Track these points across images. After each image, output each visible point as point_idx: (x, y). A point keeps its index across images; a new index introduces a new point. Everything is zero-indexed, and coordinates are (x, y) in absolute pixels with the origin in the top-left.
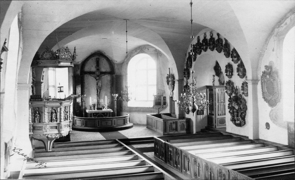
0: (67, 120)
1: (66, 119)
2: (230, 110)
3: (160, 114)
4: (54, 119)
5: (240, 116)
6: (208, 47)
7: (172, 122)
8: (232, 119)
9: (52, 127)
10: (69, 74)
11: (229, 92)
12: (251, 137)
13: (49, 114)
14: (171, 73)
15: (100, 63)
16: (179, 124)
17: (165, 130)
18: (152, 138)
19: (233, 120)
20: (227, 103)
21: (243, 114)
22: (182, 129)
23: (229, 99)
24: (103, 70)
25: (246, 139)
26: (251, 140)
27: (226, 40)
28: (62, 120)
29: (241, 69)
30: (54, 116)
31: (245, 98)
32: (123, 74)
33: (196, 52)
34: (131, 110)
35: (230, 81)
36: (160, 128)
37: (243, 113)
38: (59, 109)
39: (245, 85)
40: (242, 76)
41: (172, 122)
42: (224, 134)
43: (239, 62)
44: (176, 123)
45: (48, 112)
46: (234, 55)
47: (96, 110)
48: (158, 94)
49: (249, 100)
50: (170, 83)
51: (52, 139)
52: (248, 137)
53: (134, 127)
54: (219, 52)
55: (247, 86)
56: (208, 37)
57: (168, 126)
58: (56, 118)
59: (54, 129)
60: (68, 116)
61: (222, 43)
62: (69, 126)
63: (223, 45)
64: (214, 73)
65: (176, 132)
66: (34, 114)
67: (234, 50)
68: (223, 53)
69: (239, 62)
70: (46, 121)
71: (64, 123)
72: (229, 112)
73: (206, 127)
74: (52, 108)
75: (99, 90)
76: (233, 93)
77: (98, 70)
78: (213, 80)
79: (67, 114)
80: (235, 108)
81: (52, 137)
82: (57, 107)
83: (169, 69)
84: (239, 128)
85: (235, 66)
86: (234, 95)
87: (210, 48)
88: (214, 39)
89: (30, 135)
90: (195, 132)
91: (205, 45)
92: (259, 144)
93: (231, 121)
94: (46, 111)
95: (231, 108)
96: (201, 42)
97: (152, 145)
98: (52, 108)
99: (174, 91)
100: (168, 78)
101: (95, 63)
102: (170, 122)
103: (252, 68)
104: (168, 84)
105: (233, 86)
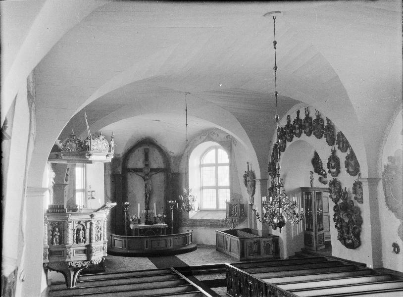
0: (100, 240)
3: (235, 230)
4: (82, 238)
6: (303, 131)
8: (339, 237)
9: (78, 252)
11: (334, 197)
12: (370, 266)
13: (74, 231)
14: (250, 170)
16: (262, 244)
17: (242, 254)
18: (224, 266)
19: (342, 239)
21: (357, 230)
24: (154, 166)
25: (362, 268)
27: (328, 120)
28: (94, 241)
29: (352, 163)
30: (81, 235)
31: (359, 205)
33: (286, 138)
34: (195, 223)
38: (88, 223)
39: (357, 186)
42: (329, 260)
44: (258, 243)
46: (345, 145)
47: (143, 225)
49: (365, 209)
50: (249, 184)
52: (365, 265)
55: (361, 187)
56: (303, 116)
64: (312, 169)
65: (259, 257)
67: (341, 135)
68: (324, 139)
69: (348, 152)
70: (70, 242)
72: (336, 226)
75: (148, 196)
77: (147, 165)
80: (344, 221)
82: (86, 222)
83: (248, 163)
85: (342, 156)
86: (341, 201)
87: (305, 132)
88: (311, 119)
95: (338, 220)
96: (292, 123)
97: (223, 276)
98: (79, 223)
100: (245, 177)
101: (143, 155)
102: (249, 241)
104: (246, 185)
105: (340, 187)
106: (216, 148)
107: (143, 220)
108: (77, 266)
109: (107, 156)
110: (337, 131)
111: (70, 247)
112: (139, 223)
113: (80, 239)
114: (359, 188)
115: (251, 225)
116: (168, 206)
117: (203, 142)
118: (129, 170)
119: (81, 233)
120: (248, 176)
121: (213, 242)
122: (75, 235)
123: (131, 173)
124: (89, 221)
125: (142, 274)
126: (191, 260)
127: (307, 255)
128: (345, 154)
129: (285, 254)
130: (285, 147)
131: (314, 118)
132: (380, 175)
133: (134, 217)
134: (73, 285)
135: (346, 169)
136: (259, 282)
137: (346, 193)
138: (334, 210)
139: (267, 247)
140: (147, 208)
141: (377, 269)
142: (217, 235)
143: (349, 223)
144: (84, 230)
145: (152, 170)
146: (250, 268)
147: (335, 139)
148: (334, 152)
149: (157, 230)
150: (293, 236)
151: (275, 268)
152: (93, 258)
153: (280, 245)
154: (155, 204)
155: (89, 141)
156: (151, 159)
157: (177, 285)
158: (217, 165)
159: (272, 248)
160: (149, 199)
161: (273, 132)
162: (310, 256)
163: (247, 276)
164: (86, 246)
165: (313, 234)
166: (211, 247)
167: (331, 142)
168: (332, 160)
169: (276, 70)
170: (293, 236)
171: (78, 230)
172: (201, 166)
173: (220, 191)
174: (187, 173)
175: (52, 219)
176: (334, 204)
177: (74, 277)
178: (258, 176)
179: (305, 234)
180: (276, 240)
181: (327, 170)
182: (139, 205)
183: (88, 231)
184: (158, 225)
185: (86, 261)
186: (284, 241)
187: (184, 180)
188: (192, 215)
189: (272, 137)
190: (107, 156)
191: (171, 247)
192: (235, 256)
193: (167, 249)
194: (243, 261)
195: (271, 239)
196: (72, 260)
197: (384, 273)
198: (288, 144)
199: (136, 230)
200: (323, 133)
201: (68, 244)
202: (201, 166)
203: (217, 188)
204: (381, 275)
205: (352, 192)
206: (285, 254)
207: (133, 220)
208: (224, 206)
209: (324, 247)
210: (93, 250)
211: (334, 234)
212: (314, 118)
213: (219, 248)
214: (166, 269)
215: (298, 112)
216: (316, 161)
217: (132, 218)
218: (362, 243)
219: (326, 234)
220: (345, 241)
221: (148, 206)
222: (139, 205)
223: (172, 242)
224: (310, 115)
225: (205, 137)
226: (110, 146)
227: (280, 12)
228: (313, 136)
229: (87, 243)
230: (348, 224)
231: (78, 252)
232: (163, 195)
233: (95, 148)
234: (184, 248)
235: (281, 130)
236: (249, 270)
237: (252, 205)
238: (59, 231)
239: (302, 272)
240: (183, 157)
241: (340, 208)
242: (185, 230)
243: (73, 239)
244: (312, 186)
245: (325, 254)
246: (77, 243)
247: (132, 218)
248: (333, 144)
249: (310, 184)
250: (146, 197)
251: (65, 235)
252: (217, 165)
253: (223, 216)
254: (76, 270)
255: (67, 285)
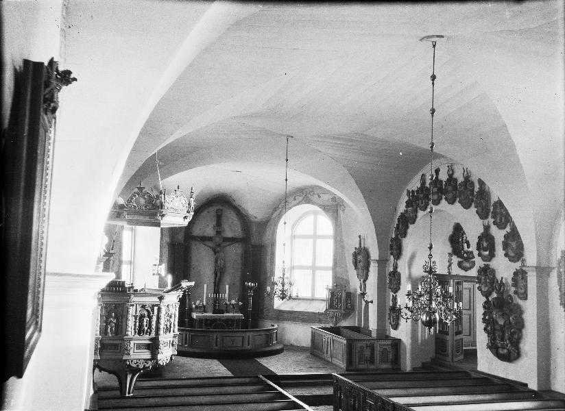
0: (170, 331)
1: (168, 330)
2: (487, 326)
3: (339, 327)
4: (146, 328)
5: (509, 339)
6: (444, 197)
7: (364, 344)
8: (490, 345)
9: (139, 346)
10: (161, 239)
11: (485, 289)
12: (533, 385)
13: (136, 319)
14: (362, 246)
15: (224, 219)
16: (378, 349)
17: (350, 362)
18: (330, 376)
19: (493, 347)
20: (480, 311)
21: (516, 336)
22: (382, 361)
23: (485, 303)
24: (229, 234)
25: (521, 389)
26: (533, 391)
27: (481, 183)
28: (161, 332)
29: (514, 244)
30: (145, 323)
31: (521, 302)
32: (266, 239)
33: (418, 206)
34: (282, 316)
35: (159, 226)
36: (340, 356)
37: (515, 333)
38: (156, 308)
39: (520, 276)
40: (514, 257)
41: (365, 346)
42: (474, 375)
43: (508, 229)
44: (372, 347)
45: (134, 314)
46: (502, 216)
47: (209, 314)
48: (336, 286)
50: (360, 265)
51: (138, 370)
52: (526, 385)
53: (285, 352)
54: (449, 203)
55: (525, 279)
56: (443, 177)
57: (356, 351)
58: (150, 327)
59: (143, 351)
60: (172, 325)
61: (473, 189)
62: (173, 345)
63: (475, 193)
64: (449, 249)
65: (372, 367)
66: (107, 318)
67: (499, 204)
68: (473, 209)
69: (508, 229)
70: (129, 333)
71: (165, 338)
72: (485, 329)
73: (431, 358)
74: (143, 307)
75: (218, 274)
76: (493, 290)
77: (218, 233)
78: (448, 264)
79: (171, 320)
80: (497, 322)
81: (138, 366)
82: (153, 306)
83: (360, 236)
84: (505, 363)
85: (499, 235)
86: (495, 295)
87: (446, 199)
88: (456, 180)
89: (94, 361)
90: (408, 368)
91: (436, 193)
92: (553, 400)
93: (487, 348)
94: (131, 312)
95: (489, 322)
96: (427, 185)
97: (329, 391)
98: (143, 307)
99: (367, 282)
100: (355, 255)
101: (215, 219)
102: (359, 344)
103: (538, 239)
104: (356, 267)
105: (494, 276)
106: (315, 213)
107: (211, 308)
108: (138, 366)
109: (185, 218)
110: (494, 199)
111: (130, 340)
112: (205, 311)
113: (144, 330)
114: (522, 279)
115: (360, 320)
116: (245, 289)
117: (298, 204)
118: (195, 238)
119: (145, 320)
120: (359, 254)
121: (306, 341)
122: (138, 324)
123: (197, 243)
124: (156, 305)
125: (218, 382)
126: (279, 366)
127: (439, 368)
128: (503, 232)
129: (408, 364)
130: (416, 217)
131: (461, 179)
132: (554, 264)
133: (198, 302)
134: (129, 393)
135: (504, 252)
136: (383, 401)
137: (502, 284)
138: (484, 307)
139: (384, 352)
140: (217, 291)
141: (541, 391)
142: (314, 335)
143: (504, 326)
144: (150, 318)
145: (226, 239)
146: (368, 381)
147: (489, 210)
148: (487, 228)
149: (230, 322)
150: (420, 341)
151: (403, 383)
152: (159, 357)
153: (402, 351)
154: (227, 286)
155: (163, 196)
156: (226, 226)
157: (271, 400)
158: (315, 237)
159: (391, 356)
160: (220, 279)
161: (399, 197)
162: (443, 369)
163: (365, 392)
164: (151, 339)
165: (449, 338)
166: (301, 349)
167: (483, 214)
168: (484, 240)
169: (433, 113)
170: (420, 341)
171: (142, 317)
172: (293, 237)
173: (318, 273)
174: (273, 244)
175: (108, 299)
176: (484, 299)
177: (131, 381)
178: (374, 254)
179: (437, 339)
180: (397, 343)
181: (476, 253)
182: (205, 286)
183: (154, 319)
184: (231, 314)
185: (150, 360)
186: (406, 344)
187: (268, 258)
188: (278, 304)
189: (397, 202)
190: (185, 218)
191: (249, 347)
192: (338, 364)
193: (243, 348)
194: (351, 371)
195: (389, 342)
196: (132, 357)
197: (552, 397)
198: (421, 214)
199: (201, 320)
200: (472, 201)
201: (127, 335)
202: (293, 237)
203: (314, 268)
204: (548, 400)
205: (510, 284)
206: (408, 364)
207: (196, 307)
208: (325, 295)
209: (462, 357)
210: (161, 346)
211: (482, 339)
212: (461, 179)
213: (315, 350)
214: (251, 377)
215: (437, 171)
216: (457, 238)
217: (195, 304)
218: (523, 354)
219: (466, 339)
220: (497, 350)
221: (217, 288)
222: (205, 286)
223: (250, 339)
224: (455, 176)
225: (301, 198)
226: (189, 204)
227: (442, 37)
228: (457, 204)
229: (153, 335)
230: (502, 327)
231: (139, 346)
232: (239, 274)
233: (171, 206)
234: (270, 349)
235: (411, 194)
236: (368, 384)
237: (363, 294)
238: (116, 317)
239: (440, 390)
240: (269, 222)
241: (494, 306)
242: (268, 325)
243: (135, 329)
244: (449, 273)
245: (466, 367)
246: (139, 334)
247: (195, 304)
248: (486, 217)
249: (447, 270)
250: (216, 275)
251: (124, 324)
252: (315, 237)
253: (321, 307)
254: (134, 371)
255: (121, 392)
